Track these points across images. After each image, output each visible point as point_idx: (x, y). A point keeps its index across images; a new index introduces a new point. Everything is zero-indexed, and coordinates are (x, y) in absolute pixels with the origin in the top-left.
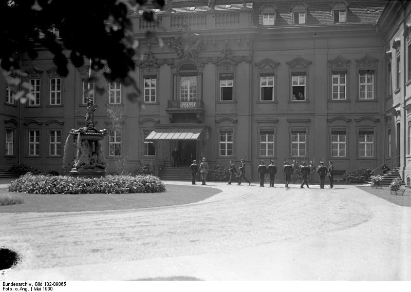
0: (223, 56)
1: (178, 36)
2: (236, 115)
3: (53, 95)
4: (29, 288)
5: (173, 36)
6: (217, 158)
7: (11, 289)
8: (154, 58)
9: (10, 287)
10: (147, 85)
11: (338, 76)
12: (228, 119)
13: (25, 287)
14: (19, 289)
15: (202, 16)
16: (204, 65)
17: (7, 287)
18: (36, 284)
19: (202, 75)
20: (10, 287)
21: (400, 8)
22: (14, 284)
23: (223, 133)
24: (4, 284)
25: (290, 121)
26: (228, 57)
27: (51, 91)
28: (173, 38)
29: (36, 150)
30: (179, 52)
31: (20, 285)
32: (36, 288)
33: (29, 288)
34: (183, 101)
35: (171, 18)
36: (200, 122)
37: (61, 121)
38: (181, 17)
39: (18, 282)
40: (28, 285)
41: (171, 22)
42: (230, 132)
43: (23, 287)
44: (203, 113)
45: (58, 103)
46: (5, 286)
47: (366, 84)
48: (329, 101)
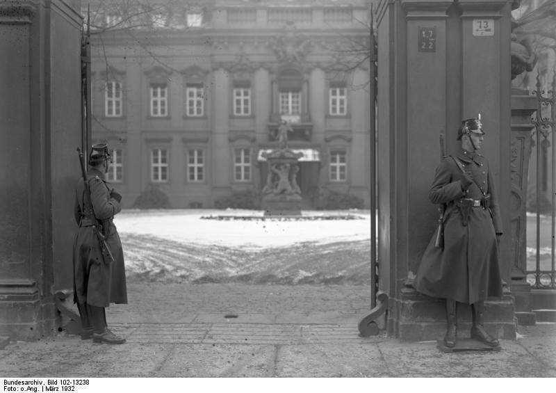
0: (335, 60)
2: (350, 131)
3: (155, 103)
4: (39, 387)
8: (247, 59)
9: (13, 386)
10: (191, 94)
11: (195, 90)
12: (339, 137)
13: (33, 386)
14: (25, 389)
16: (309, 71)
17: (10, 386)
18: (49, 382)
20: (13, 386)
22: (19, 383)
23: (333, 153)
24: (5, 382)
25: (185, 141)
27: (152, 99)
29: (117, 174)
30: (281, 53)
31: (27, 383)
32: (48, 388)
33: (39, 387)
34: (283, 113)
36: (307, 140)
37: (122, 137)
40: (37, 383)
42: (343, 153)
43: (31, 386)
44: (311, 128)
46: (7, 385)
47: (159, 99)
48: (231, 117)
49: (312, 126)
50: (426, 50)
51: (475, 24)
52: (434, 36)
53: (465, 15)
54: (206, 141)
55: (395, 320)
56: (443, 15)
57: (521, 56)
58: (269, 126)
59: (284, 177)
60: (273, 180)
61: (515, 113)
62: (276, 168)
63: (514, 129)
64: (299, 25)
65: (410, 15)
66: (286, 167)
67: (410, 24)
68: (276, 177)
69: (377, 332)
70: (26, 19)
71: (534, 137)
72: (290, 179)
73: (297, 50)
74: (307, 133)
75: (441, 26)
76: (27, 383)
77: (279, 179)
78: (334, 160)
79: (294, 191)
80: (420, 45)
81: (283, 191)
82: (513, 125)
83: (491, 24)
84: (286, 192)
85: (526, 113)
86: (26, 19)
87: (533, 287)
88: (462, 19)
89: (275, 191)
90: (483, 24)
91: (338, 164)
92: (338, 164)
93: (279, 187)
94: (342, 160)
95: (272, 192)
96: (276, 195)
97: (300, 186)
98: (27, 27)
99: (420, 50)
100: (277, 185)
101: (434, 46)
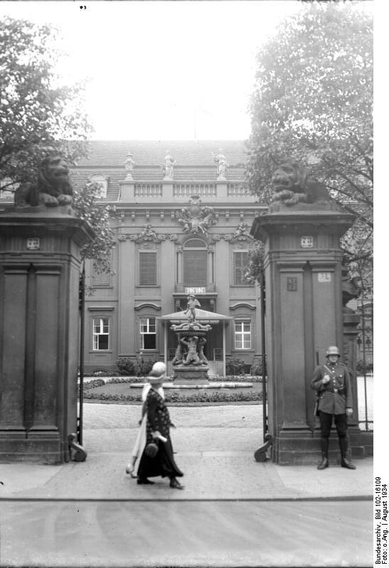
1: (185, 208)
4: (383, 528)
5: (179, 208)
6: (232, 352)
7: (385, 553)
9: (382, 555)
13: (382, 534)
14: (385, 542)
15: (157, 186)
16: (214, 242)
17: (382, 558)
18: (378, 518)
19: (213, 253)
20: (382, 555)
21: (97, 202)
22: (378, 548)
26: (244, 233)
28: (180, 210)
30: (186, 226)
31: (379, 540)
33: (383, 528)
35: (174, 187)
38: (142, 185)
39: (375, 543)
40: (379, 530)
41: (174, 191)
43: (382, 536)
44: (215, 298)
45: (104, 332)
46: (381, 561)
49: (216, 295)
50: (292, 290)
51: (320, 275)
52: (296, 282)
53: (314, 270)
54: (111, 310)
55: (276, 450)
56: (301, 270)
57: (349, 291)
58: (174, 296)
59: (192, 347)
60: (182, 352)
61: (346, 325)
62: (185, 340)
63: (345, 334)
64: (204, 199)
65: (282, 270)
66: (194, 339)
67: (282, 275)
68: (185, 349)
69: (265, 460)
70: (58, 272)
71: (362, 338)
72: (198, 351)
73: (203, 222)
74: (212, 302)
75: (300, 276)
76: (379, 540)
77: (188, 350)
78: (239, 329)
79: (202, 361)
80: (288, 287)
81: (192, 362)
82: (345, 332)
83: (329, 275)
84: (194, 363)
85: (354, 325)
86: (58, 272)
87: (364, 431)
88: (312, 272)
89: (184, 362)
90: (324, 275)
91: (243, 333)
92: (243, 333)
93: (188, 358)
94: (247, 328)
95: (181, 363)
96: (186, 365)
97: (206, 356)
98: (57, 278)
99: (288, 290)
100: (186, 356)
101: (296, 288)
